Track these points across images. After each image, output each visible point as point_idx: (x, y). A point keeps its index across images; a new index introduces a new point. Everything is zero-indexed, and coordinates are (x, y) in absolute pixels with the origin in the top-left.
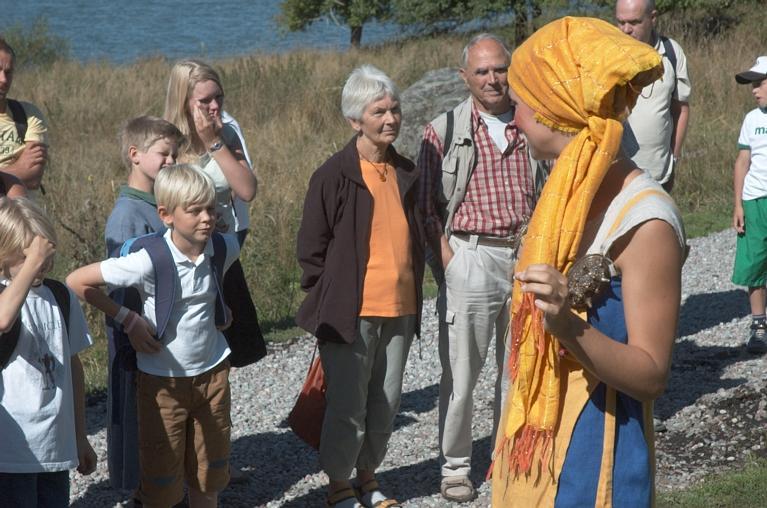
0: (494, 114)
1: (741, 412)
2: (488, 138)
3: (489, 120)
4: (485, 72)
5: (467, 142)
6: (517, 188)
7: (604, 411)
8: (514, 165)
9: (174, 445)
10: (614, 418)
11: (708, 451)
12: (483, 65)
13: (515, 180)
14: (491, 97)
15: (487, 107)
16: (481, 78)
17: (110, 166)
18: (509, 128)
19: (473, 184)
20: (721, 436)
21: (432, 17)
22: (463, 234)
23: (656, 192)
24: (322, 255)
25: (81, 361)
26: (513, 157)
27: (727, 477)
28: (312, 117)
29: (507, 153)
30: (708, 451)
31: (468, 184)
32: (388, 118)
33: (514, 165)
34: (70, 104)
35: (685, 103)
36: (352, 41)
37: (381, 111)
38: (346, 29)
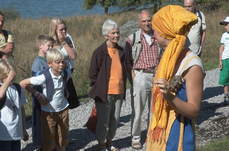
0: (148, 34)
1: (221, 122)
2: (146, 41)
3: (146, 36)
4: (145, 21)
5: (139, 42)
6: (154, 56)
7: (180, 122)
8: (153, 49)
9: (52, 132)
10: (183, 124)
11: (211, 134)
12: (144, 19)
13: (154, 54)
14: (147, 29)
15: (145, 32)
16: (144, 23)
17: (33, 49)
18: (152, 38)
19: (141, 55)
20: (215, 130)
21: (129, 5)
22: (138, 70)
23: (196, 57)
24: (96, 76)
25: (24, 107)
26: (153, 47)
27: (217, 142)
28: (93, 35)
29: (151, 46)
30: (211, 134)
31: (140, 55)
32: (116, 35)
33: (153, 49)
34: (21, 31)
35: (205, 31)
36: (105, 12)
37: (114, 33)
38: (103, 9)
